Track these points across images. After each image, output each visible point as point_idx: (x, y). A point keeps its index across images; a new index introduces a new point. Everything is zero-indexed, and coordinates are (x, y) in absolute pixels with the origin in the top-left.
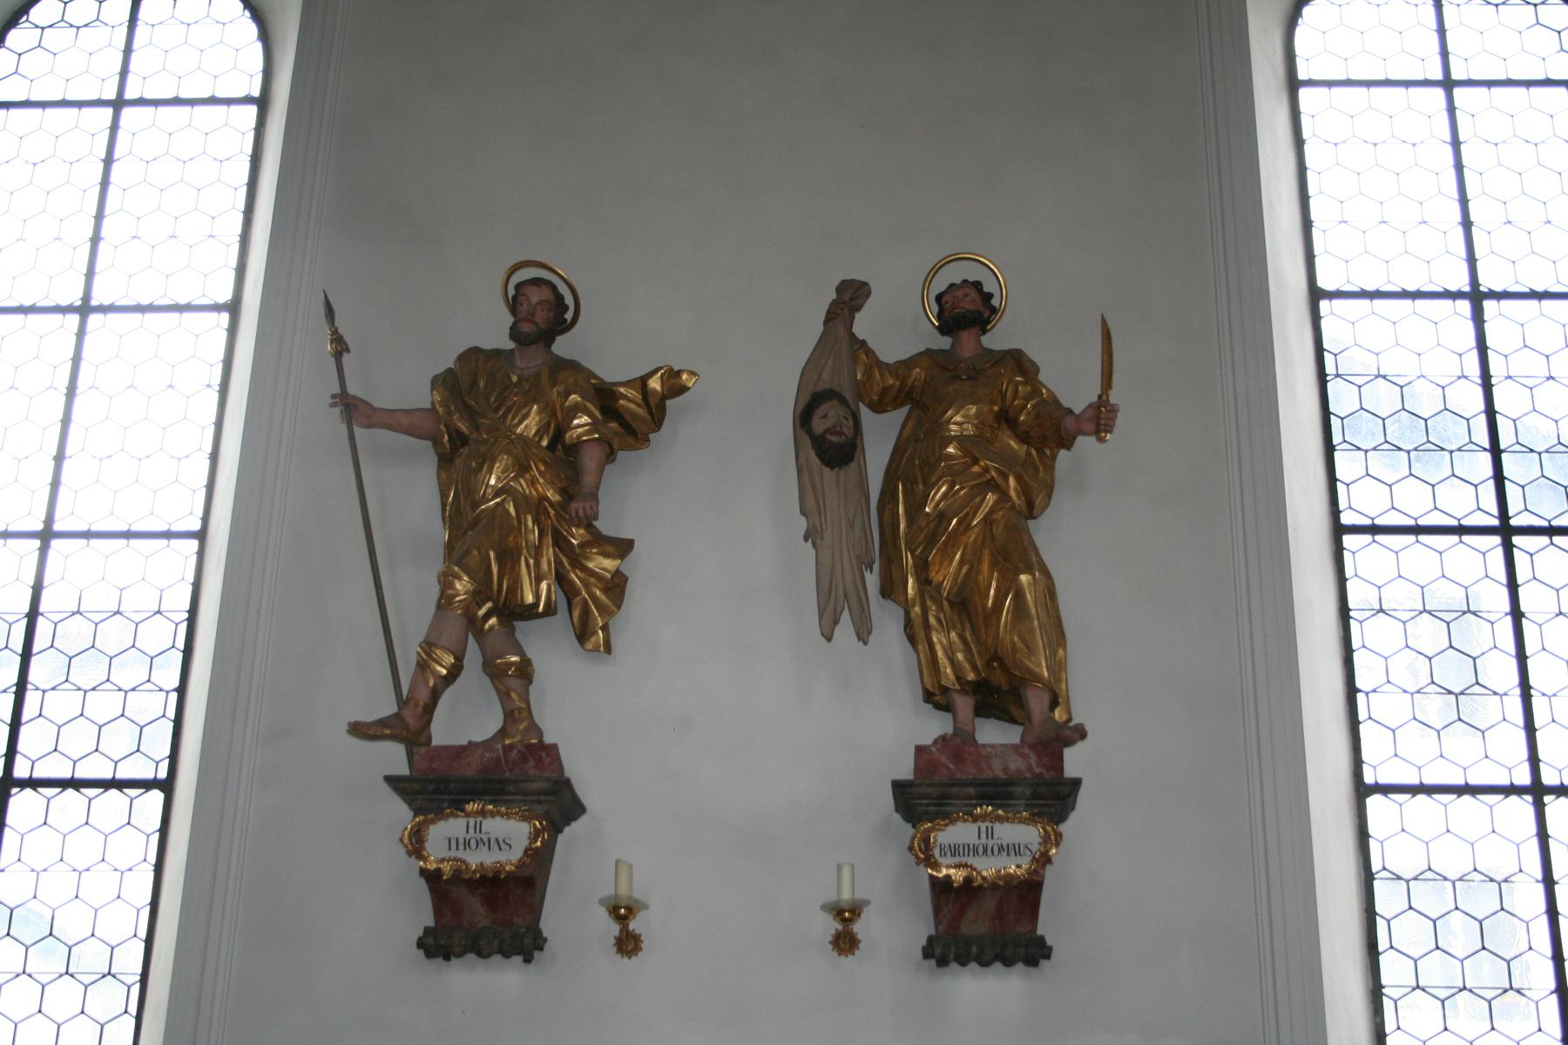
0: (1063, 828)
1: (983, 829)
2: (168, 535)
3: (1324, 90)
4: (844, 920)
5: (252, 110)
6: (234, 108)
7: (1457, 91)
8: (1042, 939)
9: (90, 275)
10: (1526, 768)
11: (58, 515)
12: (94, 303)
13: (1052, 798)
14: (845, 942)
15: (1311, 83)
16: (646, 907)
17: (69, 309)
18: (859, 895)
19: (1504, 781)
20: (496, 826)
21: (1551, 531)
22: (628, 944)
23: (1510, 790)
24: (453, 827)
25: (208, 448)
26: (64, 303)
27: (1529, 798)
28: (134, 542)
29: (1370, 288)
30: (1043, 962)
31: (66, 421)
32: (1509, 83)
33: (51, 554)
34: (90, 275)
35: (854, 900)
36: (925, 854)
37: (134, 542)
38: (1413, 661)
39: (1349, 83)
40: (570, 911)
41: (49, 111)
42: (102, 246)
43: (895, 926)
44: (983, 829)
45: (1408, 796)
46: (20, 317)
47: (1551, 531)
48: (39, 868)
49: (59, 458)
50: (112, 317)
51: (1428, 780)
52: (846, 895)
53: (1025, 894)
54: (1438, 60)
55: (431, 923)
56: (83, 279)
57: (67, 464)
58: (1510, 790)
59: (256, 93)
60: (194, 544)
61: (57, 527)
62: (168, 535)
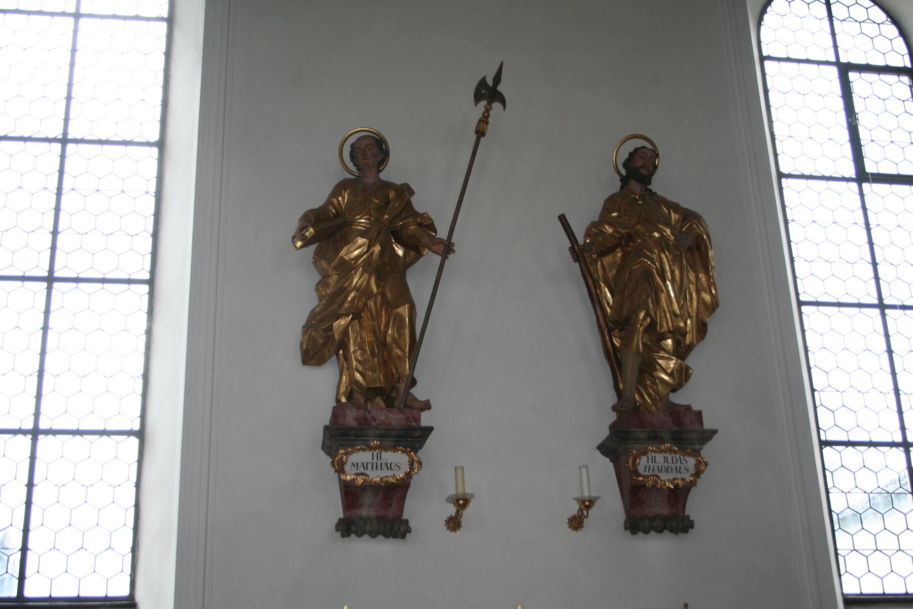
0: (420, 453)
1: (375, 454)
2: (129, 281)
3: (815, 66)
4: (459, 505)
5: (164, 26)
6: (152, 23)
7: (73, 11)
8: (688, 517)
9: (67, 120)
10: (899, 433)
11: (56, 268)
12: (69, 137)
13: (413, 437)
14: (576, 523)
15: (769, 58)
16: (473, 496)
17: (54, 140)
18: (593, 494)
19: (889, 440)
20: (390, 456)
21: (904, 307)
22: (454, 523)
23: (892, 445)
24: (361, 457)
25: (150, 229)
26: (51, 136)
27: (902, 449)
28: (82, 285)
29: (827, 175)
30: (691, 530)
31: (57, 209)
32: (808, 61)
33: (54, 292)
34: (67, 120)
35: (590, 496)
36: (340, 468)
37: (132, 286)
38: (845, 375)
39: (808, 61)
40: (424, 509)
41: (8, 15)
42: (73, 102)
43: (612, 505)
44: (375, 454)
45: (844, 447)
46: (22, 143)
47: (904, 307)
48: (846, 491)
49: (55, 233)
50: (82, 146)
51: (852, 439)
52: (586, 494)
53: (678, 495)
54: (832, 50)
55: (342, 516)
56: (63, 122)
57: (59, 237)
58: (892, 445)
59: (166, 15)
60: (146, 288)
61: (56, 275)
62: (129, 281)
